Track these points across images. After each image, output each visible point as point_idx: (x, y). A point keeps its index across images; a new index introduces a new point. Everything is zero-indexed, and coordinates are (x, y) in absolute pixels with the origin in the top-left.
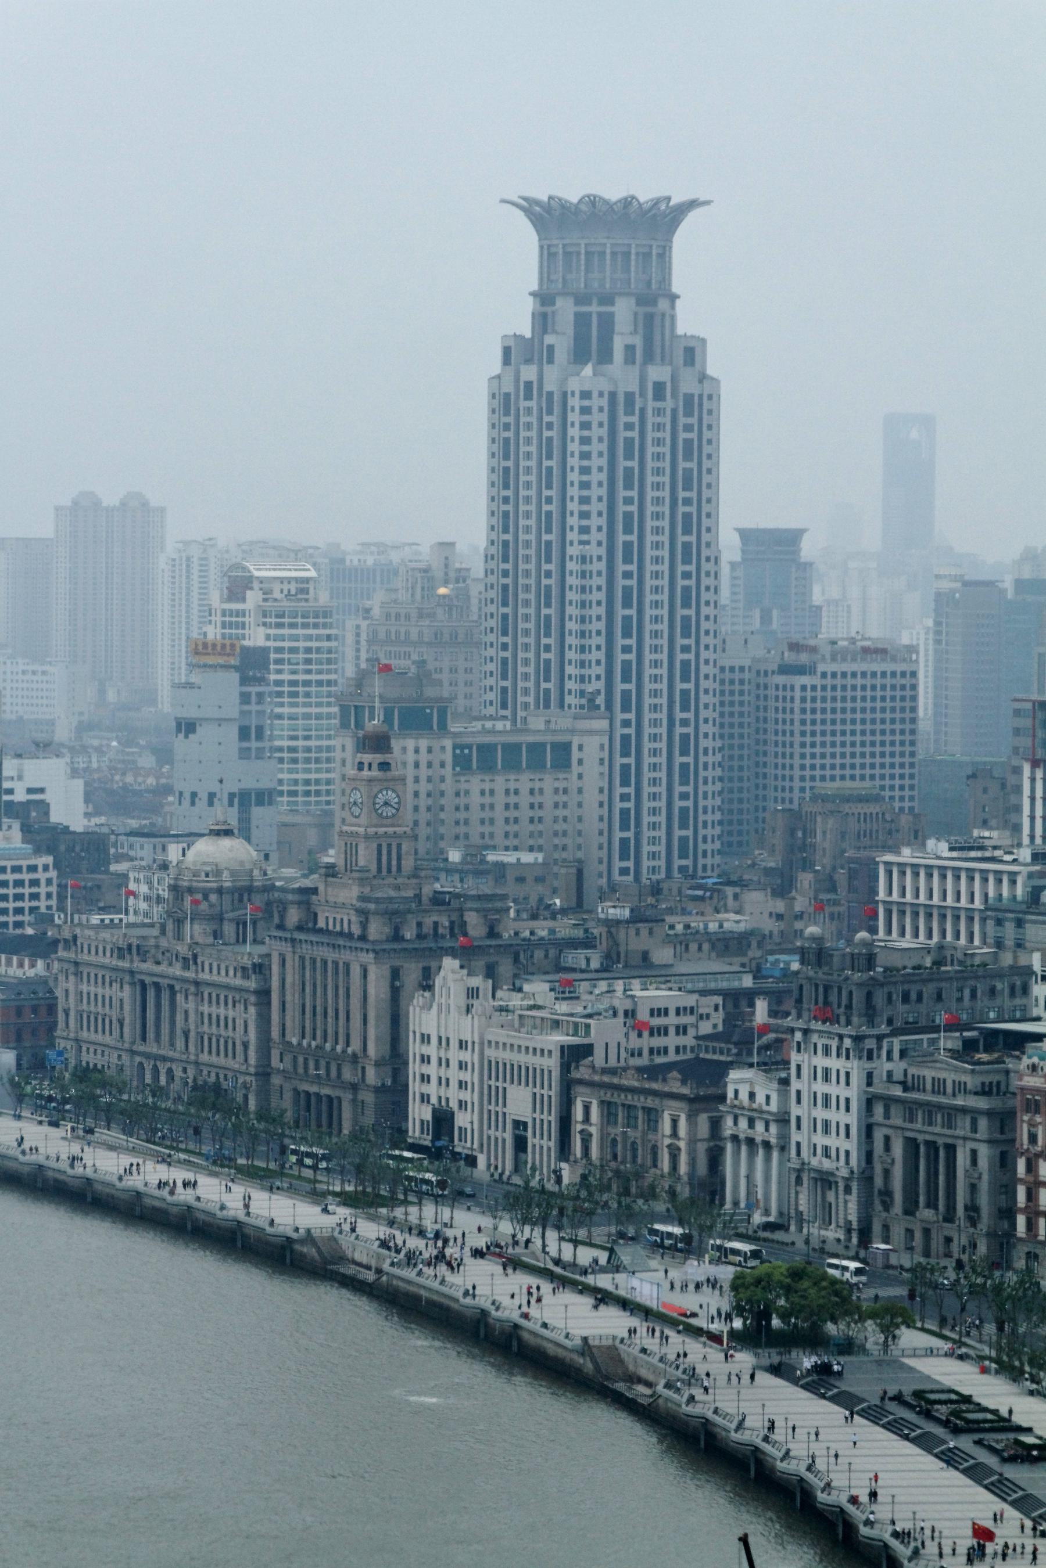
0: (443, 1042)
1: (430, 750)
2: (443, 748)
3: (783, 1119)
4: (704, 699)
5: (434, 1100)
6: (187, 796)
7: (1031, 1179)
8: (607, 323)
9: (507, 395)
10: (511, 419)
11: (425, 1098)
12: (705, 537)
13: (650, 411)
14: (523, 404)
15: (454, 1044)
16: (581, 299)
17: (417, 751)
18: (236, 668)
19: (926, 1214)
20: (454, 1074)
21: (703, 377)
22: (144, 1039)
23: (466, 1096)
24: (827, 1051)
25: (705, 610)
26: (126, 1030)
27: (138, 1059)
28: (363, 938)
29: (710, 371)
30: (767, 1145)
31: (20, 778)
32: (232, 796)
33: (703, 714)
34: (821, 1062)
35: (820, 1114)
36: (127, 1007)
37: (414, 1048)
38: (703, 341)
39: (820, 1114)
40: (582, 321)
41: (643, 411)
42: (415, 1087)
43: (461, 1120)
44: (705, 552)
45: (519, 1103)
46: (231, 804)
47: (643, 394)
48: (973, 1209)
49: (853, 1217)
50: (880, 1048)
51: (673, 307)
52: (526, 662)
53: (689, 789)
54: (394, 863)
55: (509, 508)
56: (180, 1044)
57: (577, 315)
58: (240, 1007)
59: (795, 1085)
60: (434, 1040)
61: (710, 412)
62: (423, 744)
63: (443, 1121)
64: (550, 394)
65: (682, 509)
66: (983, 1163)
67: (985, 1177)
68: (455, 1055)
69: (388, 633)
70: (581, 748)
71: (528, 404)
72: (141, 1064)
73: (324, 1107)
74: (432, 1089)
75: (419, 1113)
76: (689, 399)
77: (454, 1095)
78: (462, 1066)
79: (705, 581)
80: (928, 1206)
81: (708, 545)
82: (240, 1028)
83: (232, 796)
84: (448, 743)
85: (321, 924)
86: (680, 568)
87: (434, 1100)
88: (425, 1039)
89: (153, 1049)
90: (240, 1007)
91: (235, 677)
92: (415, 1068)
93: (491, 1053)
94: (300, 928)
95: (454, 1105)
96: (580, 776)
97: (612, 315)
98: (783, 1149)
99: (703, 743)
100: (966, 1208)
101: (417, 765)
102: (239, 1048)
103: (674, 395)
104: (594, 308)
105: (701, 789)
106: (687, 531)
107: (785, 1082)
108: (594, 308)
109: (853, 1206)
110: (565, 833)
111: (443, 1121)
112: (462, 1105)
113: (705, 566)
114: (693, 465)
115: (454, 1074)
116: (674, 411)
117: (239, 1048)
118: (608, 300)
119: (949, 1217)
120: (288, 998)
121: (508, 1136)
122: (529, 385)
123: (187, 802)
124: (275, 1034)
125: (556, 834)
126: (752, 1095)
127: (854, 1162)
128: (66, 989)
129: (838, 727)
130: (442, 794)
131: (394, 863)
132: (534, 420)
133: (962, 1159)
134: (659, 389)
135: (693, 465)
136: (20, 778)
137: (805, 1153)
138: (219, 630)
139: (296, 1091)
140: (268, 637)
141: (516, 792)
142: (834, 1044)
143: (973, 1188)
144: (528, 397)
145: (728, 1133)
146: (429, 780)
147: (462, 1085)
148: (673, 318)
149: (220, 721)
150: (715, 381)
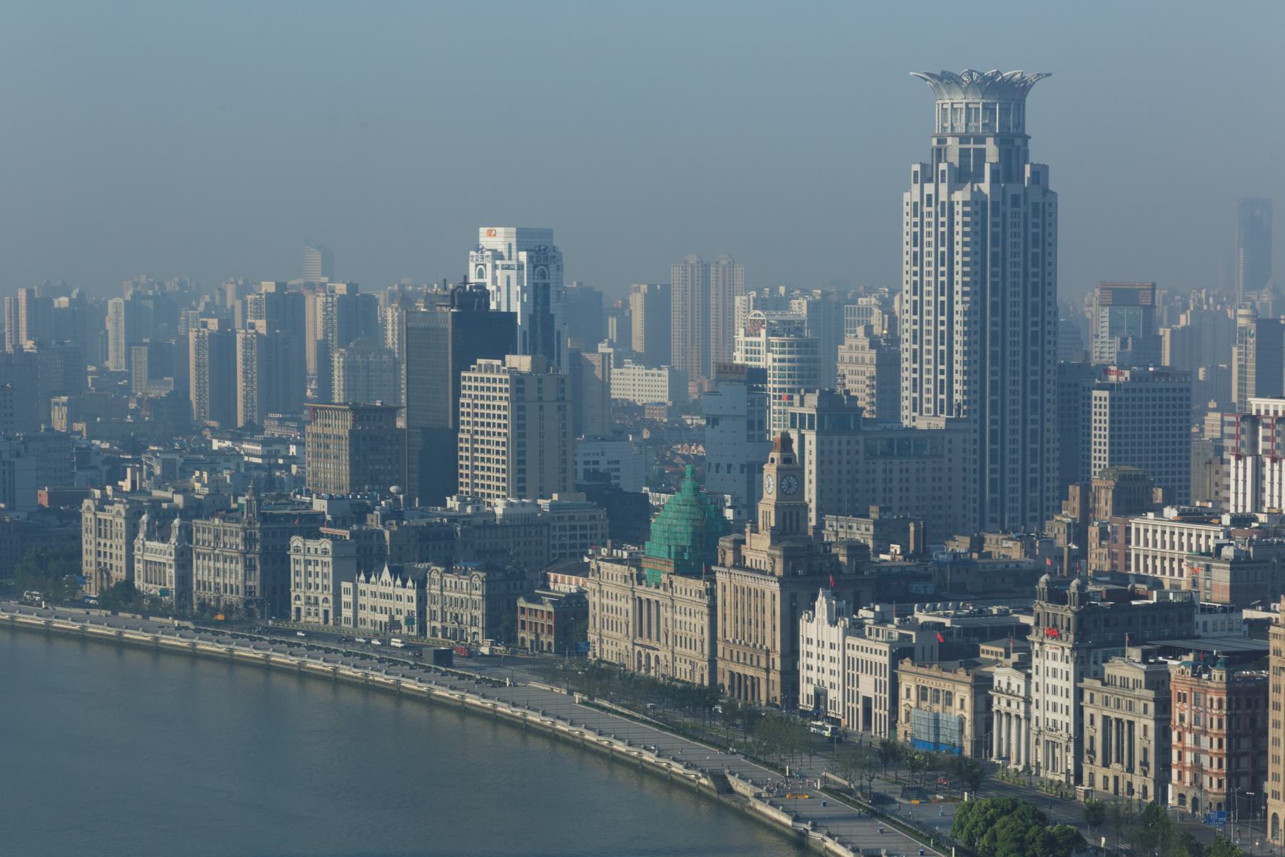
0: (821, 644)
1: (849, 443)
2: (858, 442)
3: (1028, 701)
4: (1047, 406)
5: (815, 682)
6: (714, 466)
7: (1180, 745)
8: (981, 155)
9: (916, 204)
10: (918, 220)
11: (809, 680)
12: (1048, 298)
13: (1009, 215)
14: (926, 209)
15: (827, 645)
16: (963, 139)
17: (840, 443)
18: (745, 383)
19: (1115, 766)
20: (826, 664)
21: (1046, 191)
22: (641, 635)
23: (834, 679)
24: (1055, 658)
25: (1047, 347)
26: (631, 629)
27: (637, 648)
28: (772, 574)
29: (1051, 187)
30: (1018, 717)
31: (603, 454)
32: (742, 466)
33: (1047, 415)
34: (1050, 664)
35: (1051, 698)
36: (630, 614)
37: (803, 647)
38: (1047, 167)
39: (1051, 698)
40: (964, 154)
41: (1004, 214)
42: (803, 673)
43: (833, 695)
44: (1048, 309)
45: (867, 686)
46: (742, 472)
47: (1004, 203)
48: (1145, 763)
49: (1071, 767)
50: (1089, 656)
51: (1026, 144)
52: (929, 332)
53: (1037, 465)
54: (794, 524)
55: (917, 278)
56: (663, 640)
57: (961, 150)
58: (698, 616)
59: (1035, 679)
60: (815, 642)
61: (1050, 215)
62: (845, 438)
63: (820, 696)
64: (943, 203)
65: (1031, 280)
66: (1151, 734)
67: (1153, 743)
68: (827, 652)
69: (851, 358)
70: (950, 441)
71: (929, 209)
72: (639, 653)
73: (749, 683)
74: (813, 675)
75: (806, 690)
76: (1035, 206)
77: (827, 679)
78: (832, 660)
79: (1048, 328)
80: (1118, 761)
81: (1049, 304)
82: (698, 630)
83: (742, 466)
84: (861, 438)
85: (748, 563)
86: (1030, 320)
87: (815, 682)
88: (809, 641)
89: (647, 642)
90: (698, 616)
91: (744, 388)
92: (803, 660)
93: (849, 652)
94: (734, 567)
95: (827, 685)
96: (950, 460)
97: (984, 150)
98: (1028, 719)
99: (1046, 435)
100: (1141, 764)
101: (840, 452)
102: (699, 644)
103: (1025, 204)
104: (972, 146)
105: (1046, 465)
106: (1035, 294)
107: (1029, 677)
108: (972, 146)
109: (1071, 761)
110: (940, 498)
111: (820, 696)
112: (832, 685)
113: (1047, 318)
114: (1039, 250)
115: (826, 664)
116: (1026, 214)
117: (699, 644)
118: (980, 140)
119: (1131, 770)
120: (728, 612)
121: (860, 706)
122: (929, 197)
123: (713, 470)
124: (720, 635)
125: (934, 498)
126: (1009, 684)
127: (1071, 730)
128: (593, 599)
129: (1164, 417)
130: (857, 471)
131: (794, 524)
132: (932, 220)
133: (1138, 732)
134: (1015, 200)
135: (1039, 250)
136: (603, 454)
137: (1041, 724)
138: (744, 355)
139: (732, 674)
140: (774, 360)
141: (907, 471)
142: (1059, 652)
143: (1145, 750)
144: (929, 205)
145: (994, 709)
146: (848, 462)
147: (832, 672)
148: (1026, 152)
149: (734, 417)
150: (1055, 194)
